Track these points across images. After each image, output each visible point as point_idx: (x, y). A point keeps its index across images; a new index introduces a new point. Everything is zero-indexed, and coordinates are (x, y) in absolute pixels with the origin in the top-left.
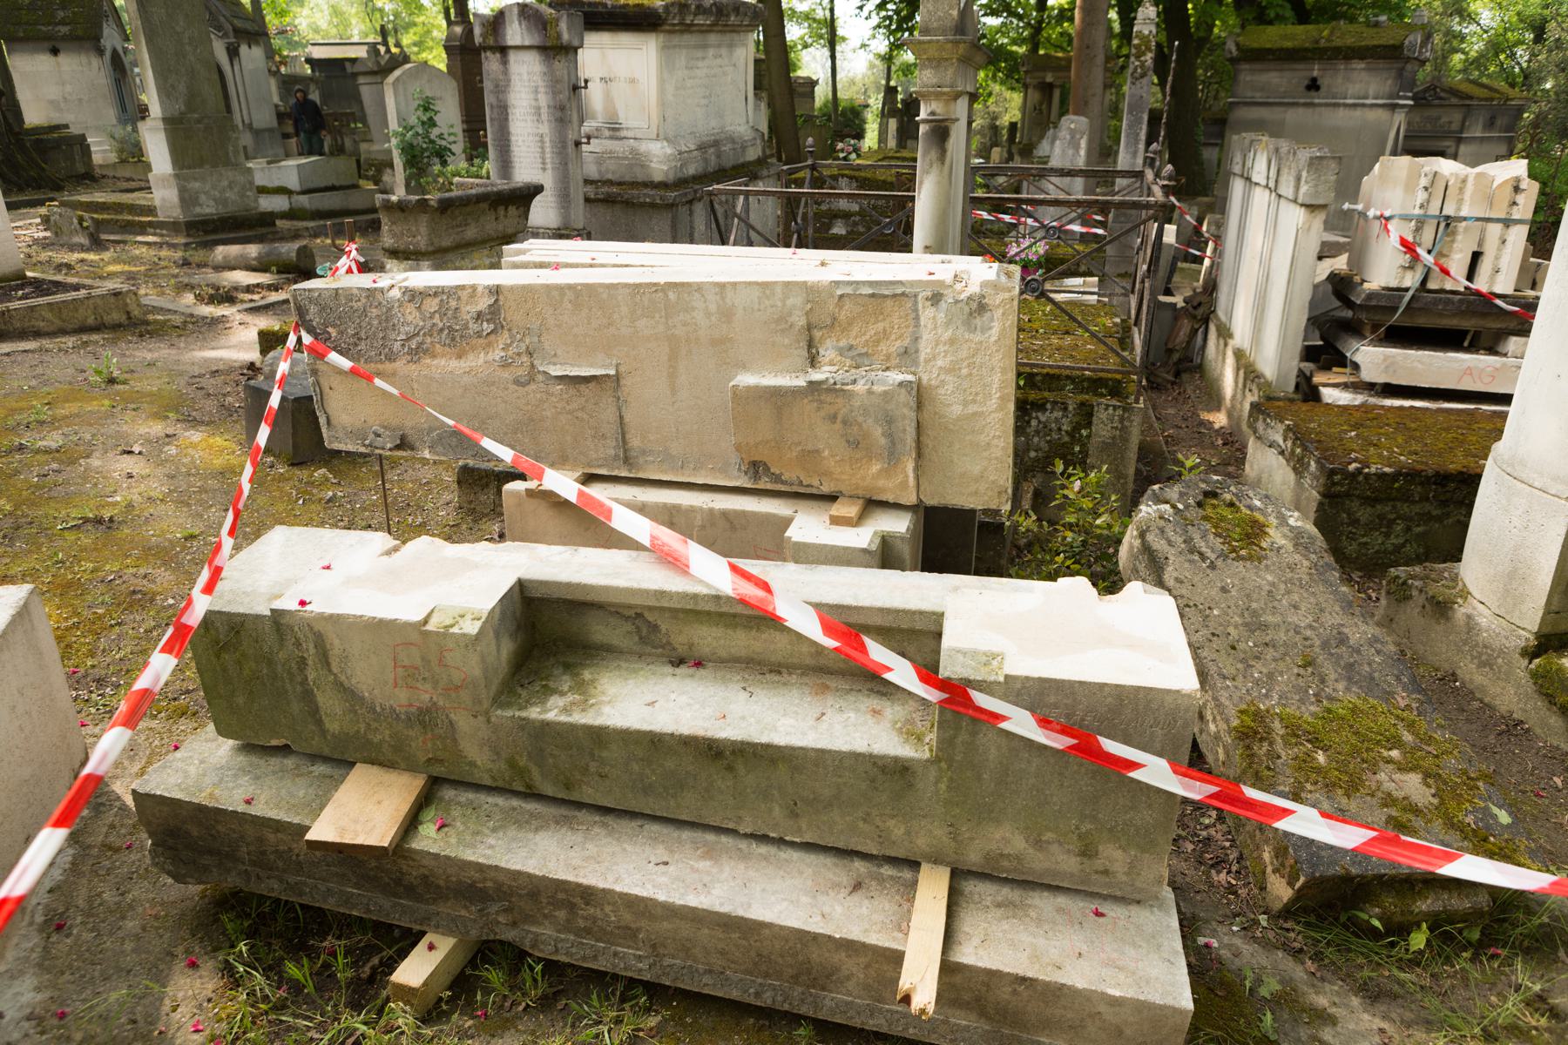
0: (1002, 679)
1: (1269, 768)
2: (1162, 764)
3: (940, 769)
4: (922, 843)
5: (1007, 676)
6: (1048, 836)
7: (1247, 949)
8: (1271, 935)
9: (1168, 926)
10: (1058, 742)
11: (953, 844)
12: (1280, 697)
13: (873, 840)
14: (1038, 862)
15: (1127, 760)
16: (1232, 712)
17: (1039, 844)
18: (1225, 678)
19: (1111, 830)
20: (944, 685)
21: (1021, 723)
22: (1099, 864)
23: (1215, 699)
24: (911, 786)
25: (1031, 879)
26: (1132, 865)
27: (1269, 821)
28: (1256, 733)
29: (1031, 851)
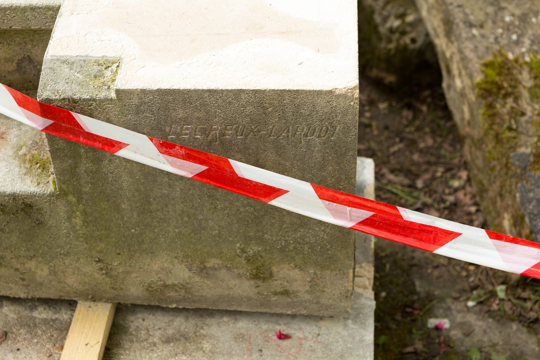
0: (113, 95)
1: (510, 129)
2: (307, 187)
3: (69, 203)
4: (72, 282)
5: (118, 92)
6: (212, 262)
7: (478, 324)
8: (507, 307)
9: (361, 341)
10: (188, 169)
11: (108, 280)
12: (533, 42)
13: (16, 283)
14: (207, 289)
15: (265, 186)
16: (476, 65)
17: (203, 271)
18: (471, 25)
19: (282, 250)
20: (46, 109)
21: (139, 149)
22: (276, 285)
23: (460, 51)
24: (40, 223)
25: (204, 306)
26: (313, 283)
27: (430, 247)
28: (500, 88)
29: (197, 279)
